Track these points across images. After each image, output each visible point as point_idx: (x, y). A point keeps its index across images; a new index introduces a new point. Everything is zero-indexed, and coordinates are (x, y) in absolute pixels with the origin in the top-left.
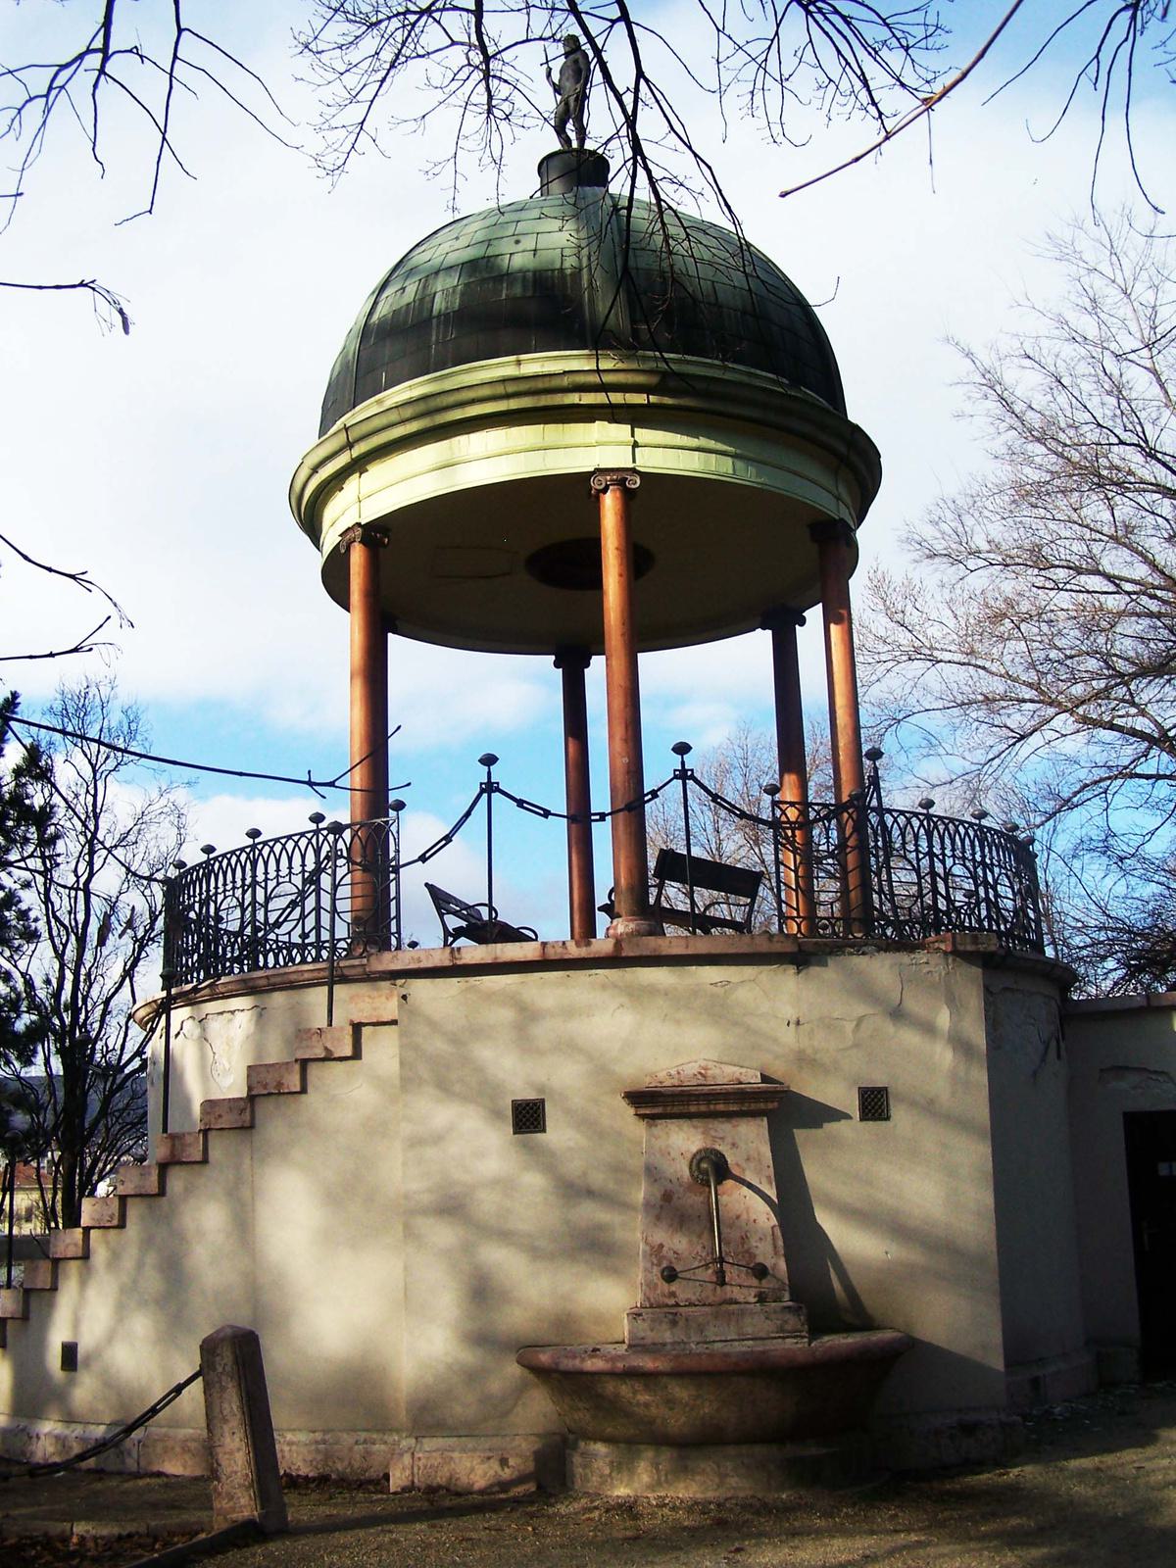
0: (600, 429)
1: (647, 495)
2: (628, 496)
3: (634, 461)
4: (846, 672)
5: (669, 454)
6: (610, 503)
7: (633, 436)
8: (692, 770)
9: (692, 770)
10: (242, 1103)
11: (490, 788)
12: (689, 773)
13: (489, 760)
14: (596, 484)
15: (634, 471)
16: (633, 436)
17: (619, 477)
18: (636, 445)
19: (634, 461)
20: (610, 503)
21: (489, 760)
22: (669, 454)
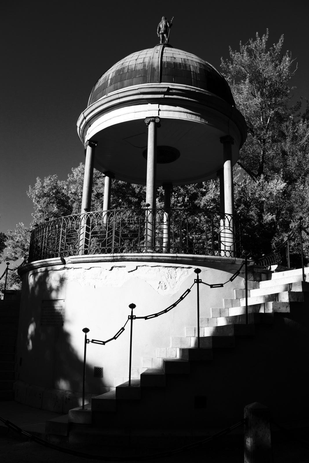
0: (149, 106)
1: (161, 124)
2: (157, 126)
3: (159, 115)
4: (89, 178)
5: (169, 112)
6: (151, 128)
7: (159, 107)
8: (201, 280)
9: (201, 280)
10: (287, 304)
11: (198, 281)
12: (200, 281)
13: (132, 306)
14: (146, 122)
15: (158, 117)
16: (159, 107)
17: (153, 119)
18: (159, 110)
19: (159, 115)
20: (151, 128)
21: (132, 306)
22: (169, 112)
